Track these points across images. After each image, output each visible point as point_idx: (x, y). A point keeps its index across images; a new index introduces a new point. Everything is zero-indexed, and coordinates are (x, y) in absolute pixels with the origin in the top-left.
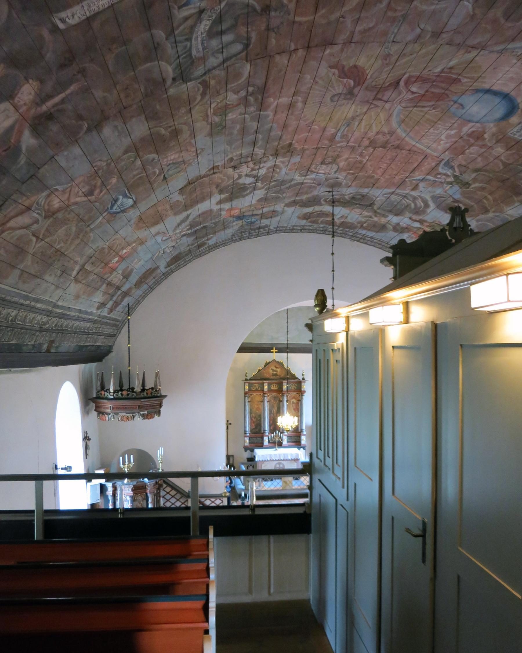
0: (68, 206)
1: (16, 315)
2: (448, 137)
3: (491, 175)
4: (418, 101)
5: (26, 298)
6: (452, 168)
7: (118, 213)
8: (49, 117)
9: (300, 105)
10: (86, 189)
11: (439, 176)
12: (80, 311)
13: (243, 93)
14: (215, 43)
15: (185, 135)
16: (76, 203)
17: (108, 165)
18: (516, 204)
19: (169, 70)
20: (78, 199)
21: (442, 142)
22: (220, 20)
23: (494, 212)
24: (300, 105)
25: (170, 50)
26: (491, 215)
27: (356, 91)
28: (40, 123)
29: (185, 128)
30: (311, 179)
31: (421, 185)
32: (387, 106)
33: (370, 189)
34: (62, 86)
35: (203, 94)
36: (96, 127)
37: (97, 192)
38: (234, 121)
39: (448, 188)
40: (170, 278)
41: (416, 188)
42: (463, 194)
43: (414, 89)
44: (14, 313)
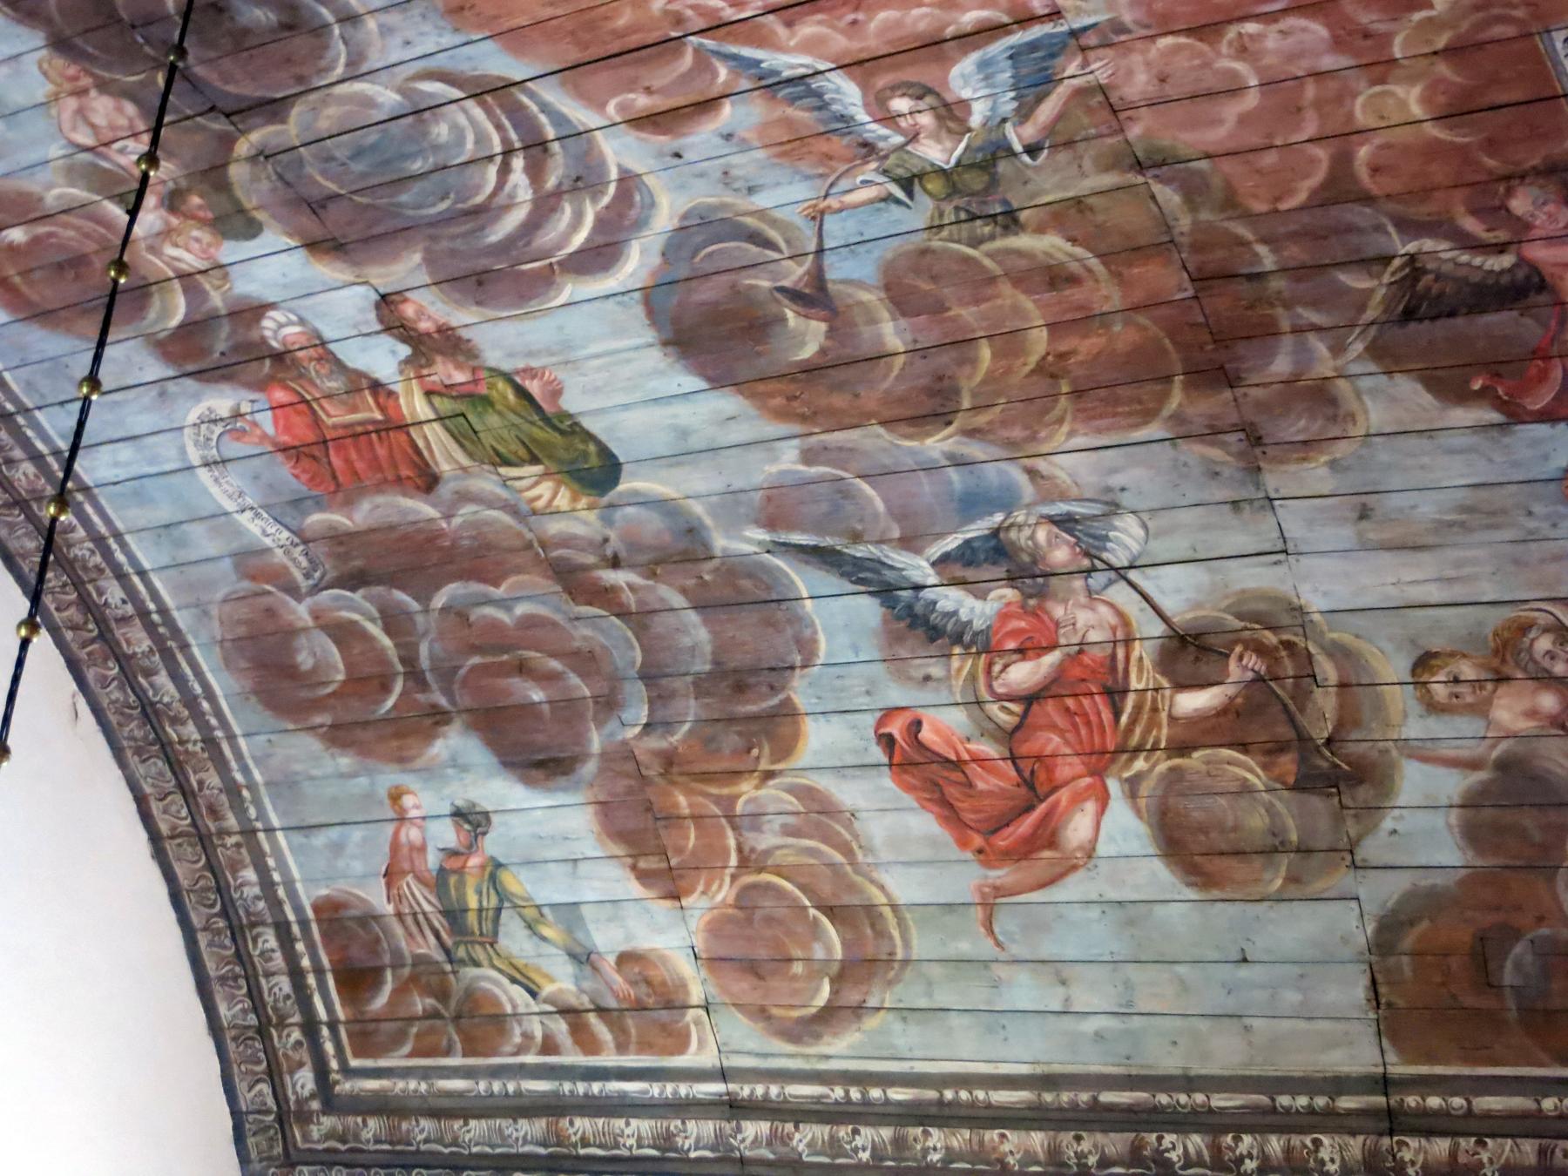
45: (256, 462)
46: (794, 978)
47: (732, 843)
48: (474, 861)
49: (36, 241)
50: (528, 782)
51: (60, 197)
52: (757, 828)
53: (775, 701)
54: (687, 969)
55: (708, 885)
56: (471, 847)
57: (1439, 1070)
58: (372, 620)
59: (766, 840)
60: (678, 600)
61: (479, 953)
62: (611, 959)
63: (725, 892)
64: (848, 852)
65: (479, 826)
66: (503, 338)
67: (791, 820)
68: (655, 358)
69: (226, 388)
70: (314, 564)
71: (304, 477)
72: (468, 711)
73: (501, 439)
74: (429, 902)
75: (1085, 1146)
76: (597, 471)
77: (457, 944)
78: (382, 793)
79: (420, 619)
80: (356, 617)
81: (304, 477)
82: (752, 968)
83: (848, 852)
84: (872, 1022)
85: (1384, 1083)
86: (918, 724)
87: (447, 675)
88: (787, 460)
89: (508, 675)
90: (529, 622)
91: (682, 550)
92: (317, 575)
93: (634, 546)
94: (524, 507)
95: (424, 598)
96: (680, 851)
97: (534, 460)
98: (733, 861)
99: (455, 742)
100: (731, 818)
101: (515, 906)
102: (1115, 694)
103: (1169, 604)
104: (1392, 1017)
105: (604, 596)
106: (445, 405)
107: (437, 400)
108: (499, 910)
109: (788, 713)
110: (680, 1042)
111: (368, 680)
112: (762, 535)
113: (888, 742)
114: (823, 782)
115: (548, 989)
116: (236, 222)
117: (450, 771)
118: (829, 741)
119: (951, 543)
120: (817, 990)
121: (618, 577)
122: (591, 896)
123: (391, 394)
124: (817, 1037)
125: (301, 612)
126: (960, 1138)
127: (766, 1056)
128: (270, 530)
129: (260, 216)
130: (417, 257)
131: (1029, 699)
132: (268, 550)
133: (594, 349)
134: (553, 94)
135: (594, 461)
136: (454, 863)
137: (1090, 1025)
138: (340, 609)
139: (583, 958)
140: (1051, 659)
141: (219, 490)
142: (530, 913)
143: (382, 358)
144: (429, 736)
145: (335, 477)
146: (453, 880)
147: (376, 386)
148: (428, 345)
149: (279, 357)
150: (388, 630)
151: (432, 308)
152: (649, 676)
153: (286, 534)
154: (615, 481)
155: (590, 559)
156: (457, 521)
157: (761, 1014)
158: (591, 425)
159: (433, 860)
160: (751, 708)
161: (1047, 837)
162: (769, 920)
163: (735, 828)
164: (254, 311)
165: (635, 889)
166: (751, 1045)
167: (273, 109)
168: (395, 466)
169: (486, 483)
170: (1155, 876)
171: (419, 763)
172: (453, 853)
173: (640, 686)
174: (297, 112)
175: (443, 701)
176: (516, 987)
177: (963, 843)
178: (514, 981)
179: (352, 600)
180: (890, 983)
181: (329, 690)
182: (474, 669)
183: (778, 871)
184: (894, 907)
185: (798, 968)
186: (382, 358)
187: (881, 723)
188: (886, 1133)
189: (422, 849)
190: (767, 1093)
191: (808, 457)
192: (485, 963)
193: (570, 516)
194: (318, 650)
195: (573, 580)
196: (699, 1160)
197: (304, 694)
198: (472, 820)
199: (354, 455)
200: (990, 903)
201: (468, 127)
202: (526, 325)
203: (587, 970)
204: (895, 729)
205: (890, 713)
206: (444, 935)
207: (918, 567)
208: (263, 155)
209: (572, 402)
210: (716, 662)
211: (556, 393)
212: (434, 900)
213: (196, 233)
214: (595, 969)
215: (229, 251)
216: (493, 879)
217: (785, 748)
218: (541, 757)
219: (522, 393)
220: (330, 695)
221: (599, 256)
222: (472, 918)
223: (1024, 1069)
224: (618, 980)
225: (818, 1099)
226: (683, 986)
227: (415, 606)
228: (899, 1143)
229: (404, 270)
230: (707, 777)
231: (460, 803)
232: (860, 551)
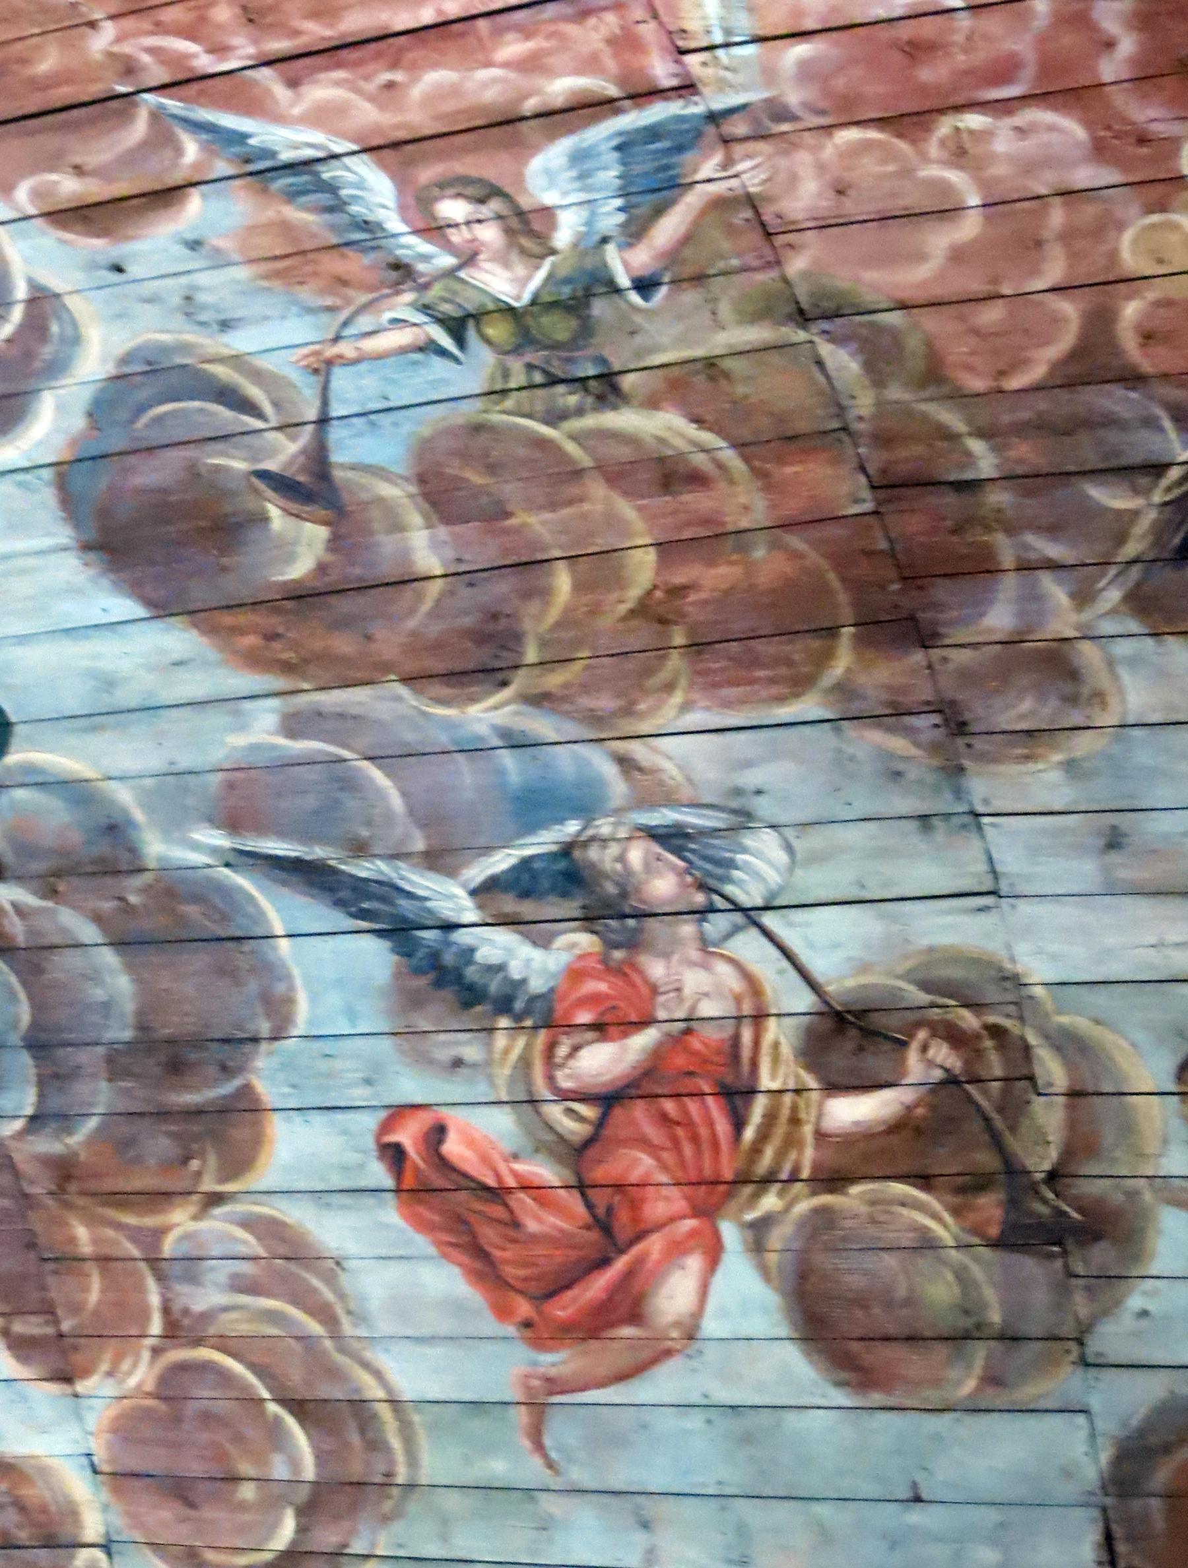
11: (453, 209)
46: (242, 1506)
52: (193, 1279)
54: (80, 1488)
59: (205, 1297)
60: (89, 932)
63: (141, 1374)
83: (326, 1315)
86: (439, 1132)
88: (262, 729)
98: (156, 1326)
100: (154, 1262)
102: (737, 1097)
109: (246, 1109)
112: (219, 839)
114: (296, 1214)
119: (501, 862)
120: (276, 1524)
131: (610, 1099)
140: (643, 1041)
161: (628, 1305)
162: (208, 1419)
163: (161, 1278)
177: (502, 1312)
180: (386, 1519)
183: (223, 1344)
184: (394, 1403)
185: (247, 1492)
187: (387, 1126)
191: (293, 725)
200: (539, 1402)
204: (406, 1136)
205: (399, 1112)
207: (449, 896)
210: (143, 1027)
217: (240, 1161)
226: (72, 1513)
232: (363, 869)
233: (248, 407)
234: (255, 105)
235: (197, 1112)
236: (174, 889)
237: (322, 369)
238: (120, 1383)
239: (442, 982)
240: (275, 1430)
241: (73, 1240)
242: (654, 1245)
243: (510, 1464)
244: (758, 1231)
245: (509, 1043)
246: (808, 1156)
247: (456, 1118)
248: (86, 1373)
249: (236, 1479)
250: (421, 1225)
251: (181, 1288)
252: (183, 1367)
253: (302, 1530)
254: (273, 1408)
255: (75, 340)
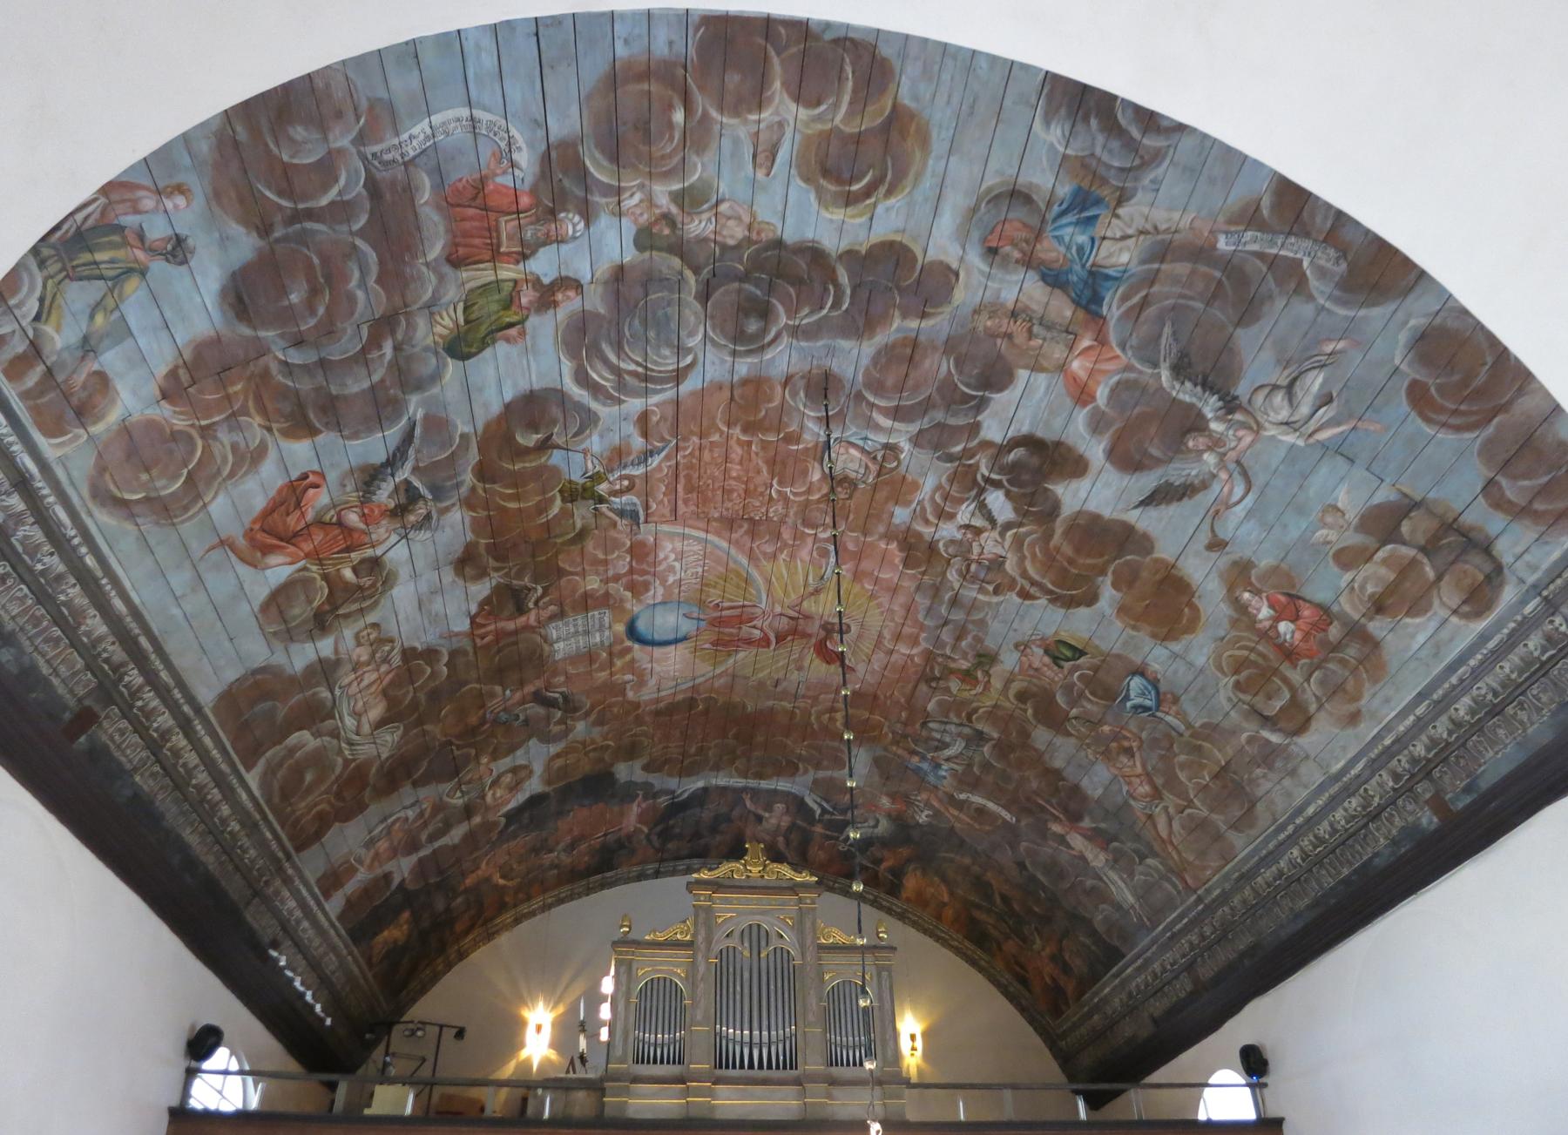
0: (1148, 774)
1: (1302, 850)
2: (671, 569)
3: (559, 541)
4: (742, 619)
5: (1282, 828)
6: (621, 513)
7: (1158, 693)
8: (1066, 811)
9: (887, 634)
10: (1124, 759)
11: (626, 483)
12: (1421, 696)
13: (942, 684)
14: (948, 739)
15: (1016, 686)
16: (1144, 766)
17: (1088, 746)
18: (470, 536)
19: (986, 749)
20: (1138, 764)
21: (673, 556)
22: (937, 749)
23: (473, 489)
24: (887, 634)
25: (977, 759)
26: (468, 478)
27: (823, 634)
28: (1074, 818)
29: (1011, 694)
30: (877, 428)
31: (638, 442)
32: (778, 609)
33: (736, 378)
34: (1043, 809)
35: (976, 710)
36: (1057, 774)
37: (1126, 744)
38: (965, 656)
39: (590, 465)
40: (973, 971)
41: (643, 419)
42: (555, 471)
43: (757, 632)
44: (1296, 852)
45: (473, 158)
46: (137, 479)
47: (217, 419)
48: (140, 254)
49: (671, 125)
50: (224, 293)
51: (695, 165)
52: (231, 430)
53: (318, 425)
54: (114, 417)
55: (181, 413)
56: (152, 251)
57: (221, 734)
58: (340, 193)
59: (225, 437)
60: (376, 378)
61: (53, 267)
62: (96, 367)
63: (180, 423)
64: (232, 475)
65: (174, 256)
66: (544, 328)
67: (243, 445)
68: (524, 386)
69: (537, 169)
70: (387, 164)
71: (460, 186)
72: (272, 251)
73: (482, 308)
74: (86, 218)
75: (110, 648)
76: (461, 346)
77: (53, 247)
78: (180, 178)
79: (345, 228)
80: (342, 181)
81: (460, 186)
82: (132, 453)
83: (232, 475)
84: (129, 527)
85: (198, 710)
86: (317, 486)
87: (303, 238)
88: (463, 427)
89: (308, 281)
90: (352, 299)
91: (406, 378)
92: (376, 163)
93: (409, 359)
94: (434, 309)
95: (361, 233)
96: (201, 392)
97: (467, 322)
98: (203, 423)
99: (245, 245)
100: (234, 414)
101: (111, 290)
102: (348, 549)
103: (391, 554)
104: (230, 699)
105: (374, 342)
106: (508, 287)
107: (511, 284)
108: (101, 277)
109: (313, 432)
110: (54, 429)
111: (286, 178)
112: (420, 415)
113: (305, 476)
114: (272, 454)
115: (48, 329)
116: (645, 239)
117: (217, 235)
118: (300, 453)
119: (417, 484)
120: (134, 492)
121: (388, 349)
122: (142, 342)
123: (518, 262)
124: (103, 505)
125: (342, 139)
126: (82, 601)
127: (72, 483)
128: (415, 143)
129: (647, 254)
130: (602, 311)
131: (340, 524)
132: (397, 135)
133: (533, 364)
134: (670, 394)
135: (466, 350)
136: (132, 239)
137: (176, 611)
138: (348, 172)
139: (88, 347)
140: (362, 526)
141: (450, 115)
142: (110, 302)
143: (544, 265)
144: (245, 222)
145: (459, 205)
146: (116, 238)
147: (524, 257)
148: (548, 295)
149: (552, 213)
150: (332, 203)
151: (569, 305)
152: (323, 363)
153: (412, 153)
154: (453, 357)
155: (399, 336)
156: (424, 269)
157: (101, 469)
158: (488, 352)
159: (129, 220)
160: (312, 416)
161: (267, 550)
162: (171, 452)
163: (227, 418)
164: (588, 216)
165: (162, 370)
166: (75, 474)
167: (705, 296)
168: (466, 246)
169: (452, 293)
170: (261, 593)
171: (217, 210)
172: (141, 236)
173: (315, 358)
174: (698, 306)
175: (277, 234)
176: (37, 305)
177: (254, 522)
178: (42, 300)
179: (357, 183)
180: (157, 523)
181: (272, 146)
182: (309, 259)
183: (207, 448)
184: (205, 505)
185: (144, 477)
186: (544, 265)
187: (314, 472)
188: (61, 568)
189: (137, 211)
190: (46, 496)
191: (463, 436)
192: (45, 273)
193: (429, 332)
194: (309, 146)
195: (384, 325)
196: (122, 694)
197: (265, 129)
198: (177, 250)
199: (476, 224)
200: (225, 543)
201: (666, 361)
202: (551, 340)
203: (79, 353)
204: (312, 478)
205: (322, 475)
206: (58, 234)
207: (405, 473)
208: (681, 280)
209: (501, 348)
210: (337, 397)
211: (508, 340)
212: (90, 222)
213: (646, 216)
214: (83, 358)
215: (629, 228)
216: (130, 271)
217: (289, 434)
218: (246, 298)
219: (511, 325)
220: (266, 145)
221: (582, 379)
222: (86, 257)
223: (137, 600)
224: (80, 378)
225: (60, 524)
226: (98, 419)
227: (356, 227)
228: (59, 578)
229: (595, 301)
230: (259, 399)
231: (190, 242)
232: (411, 452)
233: (575, 435)
234: (667, 458)
235: (305, 417)
236: (397, 407)
237: (585, 452)
238: (170, 416)
239: (370, 477)
240: (175, 477)
241: (233, 384)
242: (292, 549)
243: (197, 549)
244: (305, 569)
245: (353, 497)
246: (331, 570)
247: (324, 489)
248: (172, 403)
249: (147, 470)
250: (280, 491)
251: (225, 426)
252: (190, 438)
253: (138, 501)
254: (185, 472)
255: (604, 405)
